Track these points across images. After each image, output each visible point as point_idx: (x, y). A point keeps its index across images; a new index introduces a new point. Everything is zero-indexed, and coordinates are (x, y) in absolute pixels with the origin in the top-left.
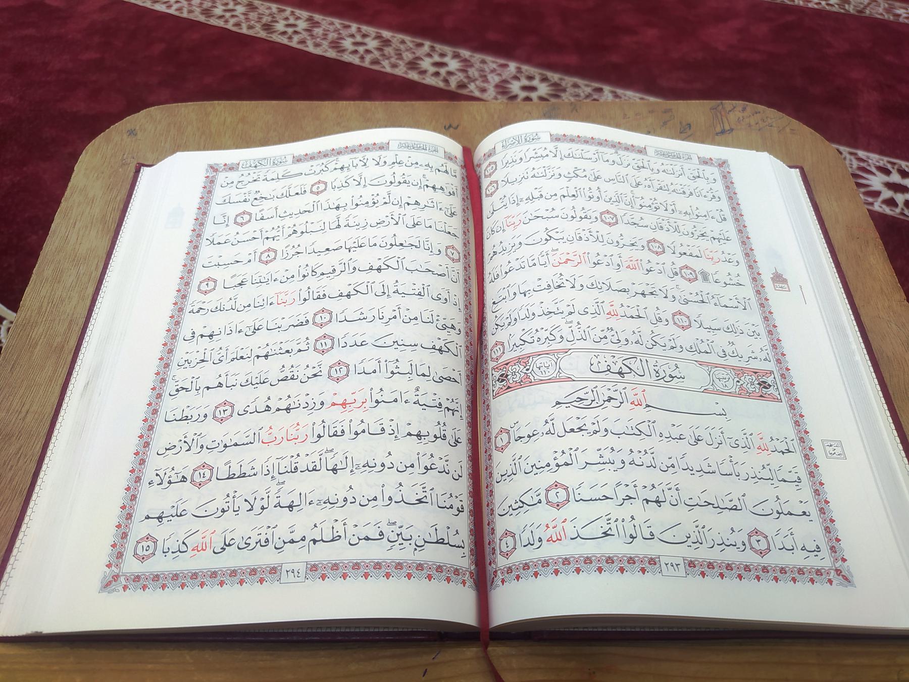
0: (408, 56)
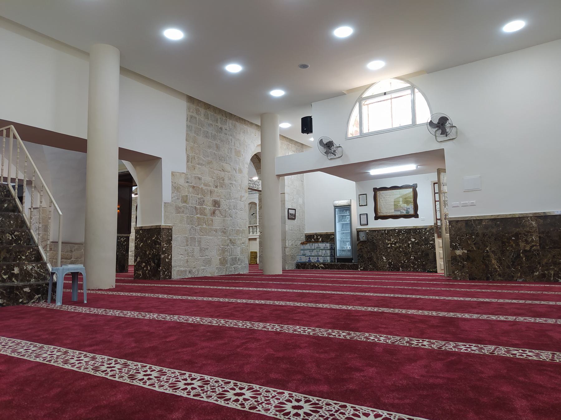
0: (219, 390)
